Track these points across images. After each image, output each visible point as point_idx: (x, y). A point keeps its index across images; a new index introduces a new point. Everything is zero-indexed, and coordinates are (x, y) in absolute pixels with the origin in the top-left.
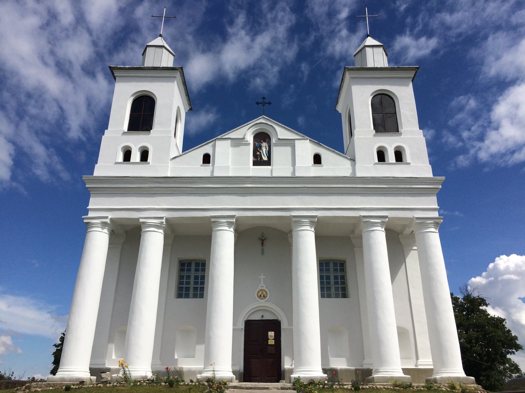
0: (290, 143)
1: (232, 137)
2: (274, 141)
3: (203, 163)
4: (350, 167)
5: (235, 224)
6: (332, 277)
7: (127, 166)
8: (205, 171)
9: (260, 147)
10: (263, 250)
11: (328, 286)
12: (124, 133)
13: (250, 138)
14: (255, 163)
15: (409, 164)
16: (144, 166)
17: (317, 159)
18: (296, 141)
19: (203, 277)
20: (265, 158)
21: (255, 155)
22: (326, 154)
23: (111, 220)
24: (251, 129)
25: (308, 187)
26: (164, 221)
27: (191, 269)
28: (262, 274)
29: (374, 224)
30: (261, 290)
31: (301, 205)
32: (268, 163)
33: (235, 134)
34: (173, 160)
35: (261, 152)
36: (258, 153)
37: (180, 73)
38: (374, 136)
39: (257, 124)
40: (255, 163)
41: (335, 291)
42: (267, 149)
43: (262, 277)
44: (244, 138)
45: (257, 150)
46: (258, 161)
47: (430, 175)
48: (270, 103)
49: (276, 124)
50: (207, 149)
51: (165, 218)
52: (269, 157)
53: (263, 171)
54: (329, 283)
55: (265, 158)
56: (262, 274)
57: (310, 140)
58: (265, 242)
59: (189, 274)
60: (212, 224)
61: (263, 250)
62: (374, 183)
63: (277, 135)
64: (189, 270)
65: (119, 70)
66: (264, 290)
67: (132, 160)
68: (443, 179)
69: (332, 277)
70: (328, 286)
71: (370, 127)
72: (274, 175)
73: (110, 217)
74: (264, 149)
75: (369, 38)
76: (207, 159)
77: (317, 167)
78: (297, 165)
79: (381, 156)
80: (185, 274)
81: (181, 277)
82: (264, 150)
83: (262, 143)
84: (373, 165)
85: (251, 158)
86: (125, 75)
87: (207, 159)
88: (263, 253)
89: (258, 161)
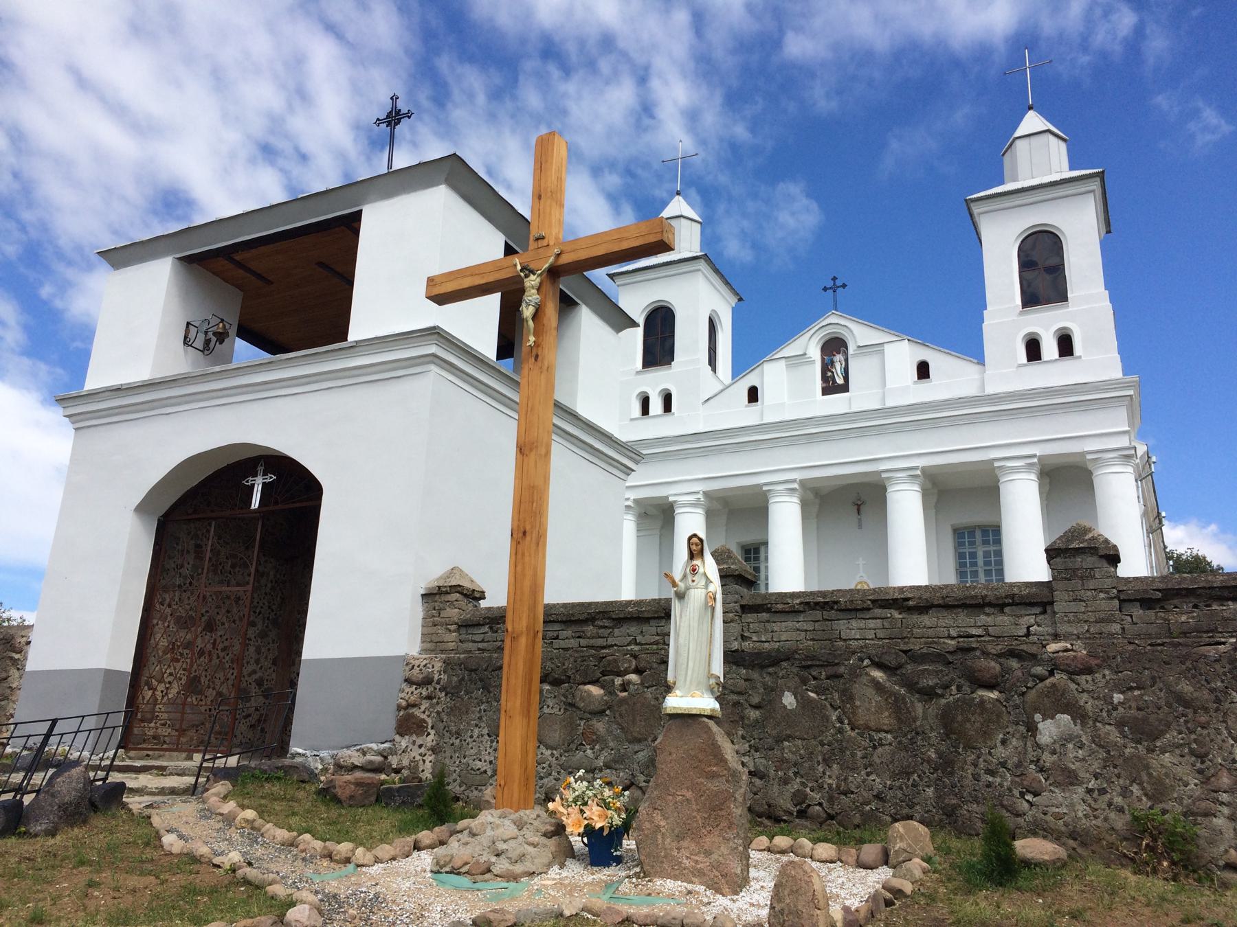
0: (876, 349)
1: (786, 356)
2: (851, 350)
3: (919, 378)
4: (977, 376)
5: (922, 477)
6: (980, 554)
7: (646, 421)
8: (750, 416)
9: (832, 363)
10: (860, 520)
11: (974, 569)
12: (638, 373)
13: (815, 353)
14: (826, 391)
15: (1080, 357)
16: (668, 418)
17: (923, 371)
18: (886, 346)
19: (999, 554)
20: (840, 381)
21: (825, 378)
22: (937, 361)
23: (635, 500)
24: (813, 338)
25: (798, 435)
26: (700, 496)
27: (975, 541)
28: (861, 559)
29: (1014, 470)
30: (860, 582)
31: (895, 452)
32: (845, 388)
33: (791, 349)
34: (706, 404)
35: (834, 370)
36: (829, 374)
37: (706, 261)
38: (1021, 314)
39: (823, 326)
40: (826, 391)
41: (986, 576)
42: (843, 365)
43: (861, 562)
44: (805, 354)
45: (827, 368)
46: (830, 387)
47: (1117, 373)
48: (844, 286)
49: (850, 319)
50: (751, 380)
51: (701, 493)
52: (846, 378)
53: (837, 404)
54: (987, 563)
55: (840, 381)
56: (861, 559)
57: (909, 340)
58: (861, 507)
59: (974, 550)
60: (997, 472)
61: (860, 520)
62: (1115, 389)
63: (856, 342)
64: (972, 543)
65: (622, 276)
66: (865, 583)
67: (651, 412)
68: (1134, 379)
69: (980, 554)
70: (974, 569)
71: (1014, 299)
72: (888, 405)
73: (632, 498)
74: (838, 366)
75: (1031, 113)
76: (753, 395)
77: (924, 384)
78: (887, 387)
79: (1033, 349)
80: (967, 550)
81: (960, 556)
82: (838, 368)
83: (834, 355)
84: (1015, 369)
85: (818, 384)
86: (632, 280)
87: (753, 395)
88: (860, 526)
89: (830, 387)
